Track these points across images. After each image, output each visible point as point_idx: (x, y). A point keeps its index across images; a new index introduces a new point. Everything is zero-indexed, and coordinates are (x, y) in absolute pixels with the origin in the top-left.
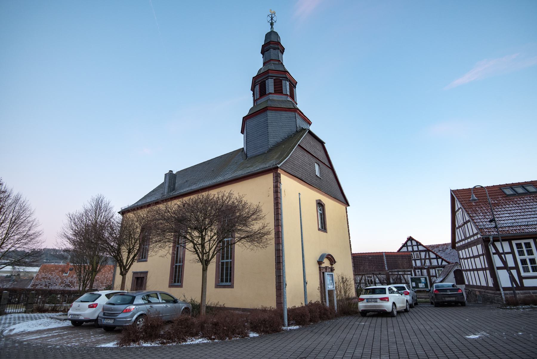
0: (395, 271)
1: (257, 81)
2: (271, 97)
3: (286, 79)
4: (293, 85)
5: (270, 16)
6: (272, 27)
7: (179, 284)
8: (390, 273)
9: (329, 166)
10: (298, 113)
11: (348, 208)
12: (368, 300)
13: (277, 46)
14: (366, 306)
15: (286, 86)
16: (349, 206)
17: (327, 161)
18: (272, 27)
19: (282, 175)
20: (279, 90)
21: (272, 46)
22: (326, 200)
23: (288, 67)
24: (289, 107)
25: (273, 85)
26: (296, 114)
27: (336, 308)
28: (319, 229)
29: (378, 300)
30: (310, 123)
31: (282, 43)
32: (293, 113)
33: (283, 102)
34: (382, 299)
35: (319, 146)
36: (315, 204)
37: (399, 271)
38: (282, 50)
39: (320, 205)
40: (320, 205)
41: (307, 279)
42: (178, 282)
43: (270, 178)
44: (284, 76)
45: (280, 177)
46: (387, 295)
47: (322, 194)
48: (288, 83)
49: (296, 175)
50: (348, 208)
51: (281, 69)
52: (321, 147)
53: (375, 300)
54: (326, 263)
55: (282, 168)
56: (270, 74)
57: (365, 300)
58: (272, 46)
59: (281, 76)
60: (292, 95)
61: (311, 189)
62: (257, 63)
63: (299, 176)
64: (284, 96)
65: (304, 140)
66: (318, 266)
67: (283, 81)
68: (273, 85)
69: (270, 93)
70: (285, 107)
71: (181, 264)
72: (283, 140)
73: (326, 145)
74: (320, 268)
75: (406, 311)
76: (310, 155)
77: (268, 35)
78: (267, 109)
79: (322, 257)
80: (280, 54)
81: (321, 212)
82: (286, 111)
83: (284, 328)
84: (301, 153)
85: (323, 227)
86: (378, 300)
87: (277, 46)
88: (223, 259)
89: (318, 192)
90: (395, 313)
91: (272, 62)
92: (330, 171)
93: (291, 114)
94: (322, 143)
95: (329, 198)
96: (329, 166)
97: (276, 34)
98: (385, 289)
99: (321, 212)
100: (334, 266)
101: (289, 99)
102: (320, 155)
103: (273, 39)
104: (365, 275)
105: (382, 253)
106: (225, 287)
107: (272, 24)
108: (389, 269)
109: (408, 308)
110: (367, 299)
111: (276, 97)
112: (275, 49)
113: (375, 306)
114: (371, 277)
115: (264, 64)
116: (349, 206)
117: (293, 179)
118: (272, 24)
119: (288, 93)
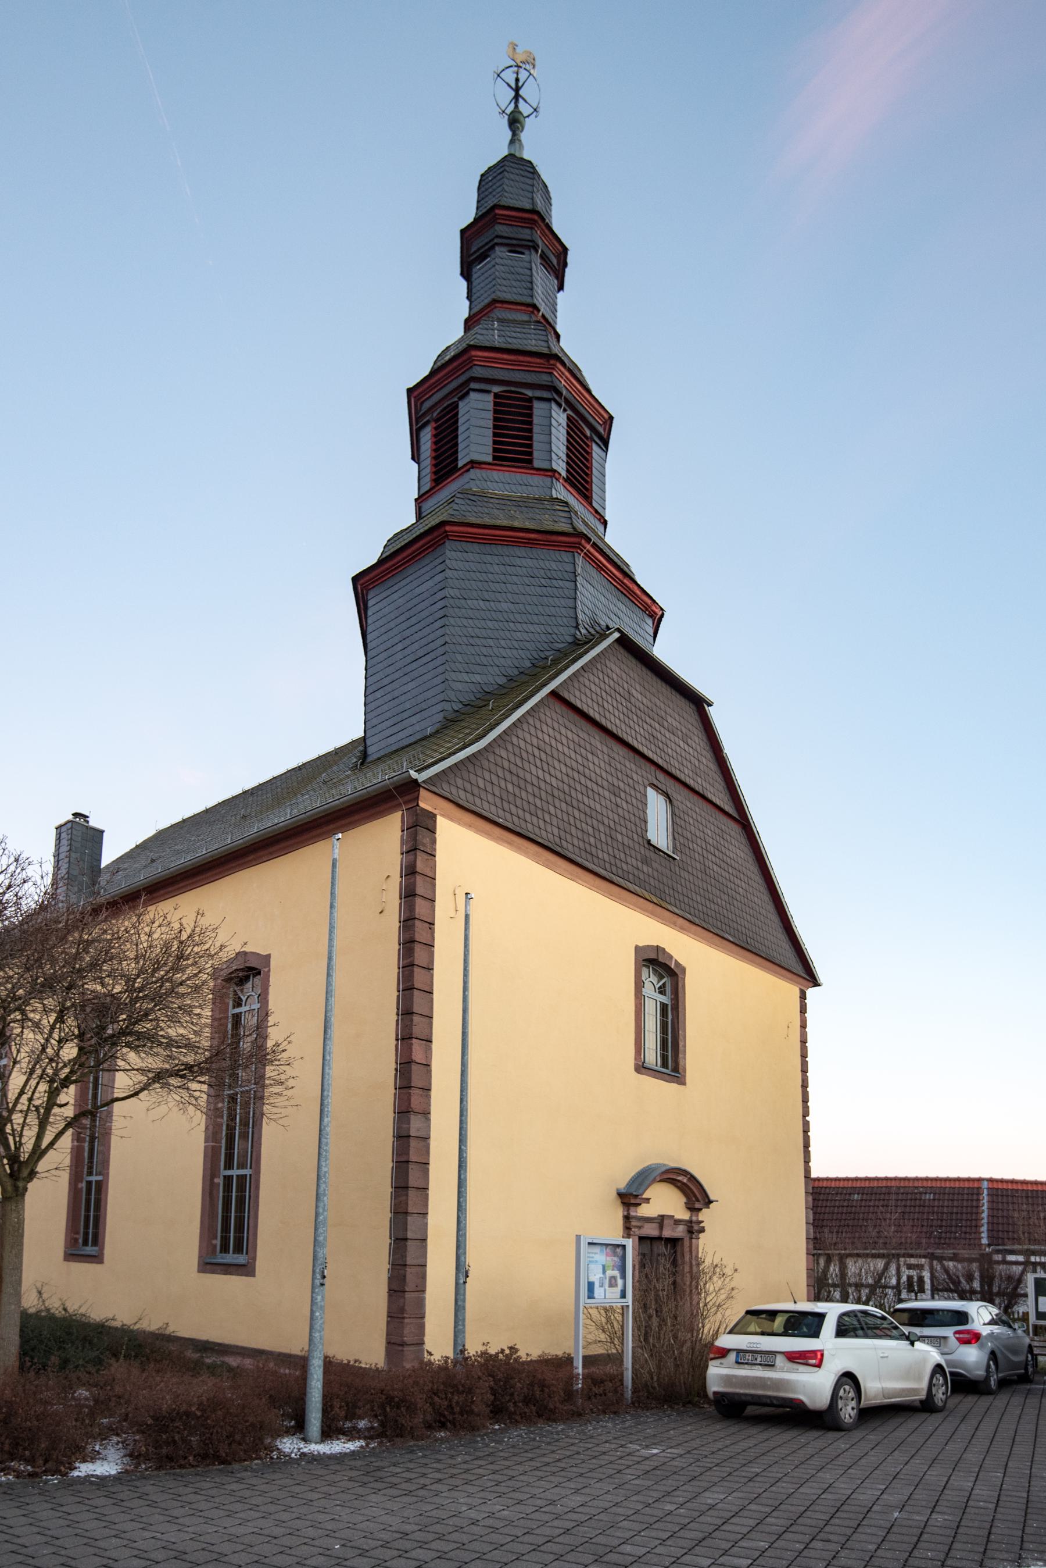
0: (1013, 1252)
1: (427, 405)
2: (474, 480)
3: (553, 393)
4: (591, 429)
5: (509, 76)
6: (515, 140)
7: (241, 1259)
8: (998, 1257)
9: (729, 808)
10: (588, 556)
11: (811, 992)
12: (743, 1357)
13: (525, 234)
14: (728, 1380)
15: (554, 430)
16: (816, 983)
17: (720, 784)
18: (515, 140)
19: (443, 824)
20: (514, 447)
21: (510, 231)
22: (684, 946)
23: (573, 344)
24: (549, 526)
25: (502, 419)
26: (580, 561)
27: (628, 1376)
28: (641, 1068)
29: (780, 1361)
30: (654, 614)
31: (562, 222)
32: (566, 557)
33: (523, 503)
34: (795, 1357)
35: (681, 714)
36: (624, 969)
37: (1034, 1253)
38: (557, 262)
39: (656, 964)
40: (656, 964)
41: (472, 1258)
42: (238, 1249)
43: (386, 835)
44: (544, 379)
45: (433, 831)
46: (827, 1340)
47: (673, 925)
48: (560, 417)
49: (530, 830)
50: (811, 992)
51: (532, 342)
52: (693, 718)
53: (767, 1359)
54: (663, 1202)
55: (445, 789)
56: (478, 372)
57: (732, 1356)
58: (510, 231)
59: (530, 378)
60: (582, 478)
61: (610, 896)
62: (436, 316)
63: (543, 837)
64: (536, 480)
65: (597, 681)
66: (620, 1213)
67: (536, 404)
68: (502, 419)
69: (474, 464)
70: (528, 525)
71: (100, 1178)
72: (511, 680)
73: (714, 713)
74: (627, 1218)
75: (927, 1406)
76: (618, 748)
77: (489, 180)
78: (446, 536)
79: (644, 1178)
80: (541, 277)
81: (664, 999)
82: (530, 543)
83: (289, 1445)
84: (562, 734)
85: (669, 1062)
86: (780, 1361)
87: (525, 234)
88: (229, 1165)
89: (652, 914)
90: (848, 1412)
91: (499, 313)
92: (734, 830)
93: (551, 561)
94: (698, 703)
95: (711, 944)
96: (729, 808)
97: (528, 169)
98: (821, 1317)
99: (664, 999)
100: (705, 1215)
101: (561, 491)
102: (687, 757)
103: (514, 196)
104: (898, 1256)
105: (980, 1180)
106: (228, 1269)
107: (515, 122)
108: (994, 1240)
109: (939, 1395)
110: (739, 1351)
111: (503, 483)
112: (517, 247)
113: (762, 1382)
114: (920, 1267)
115: (469, 324)
116: (816, 983)
117: (510, 844)
118: (515, 122)
119: (560, 466)
